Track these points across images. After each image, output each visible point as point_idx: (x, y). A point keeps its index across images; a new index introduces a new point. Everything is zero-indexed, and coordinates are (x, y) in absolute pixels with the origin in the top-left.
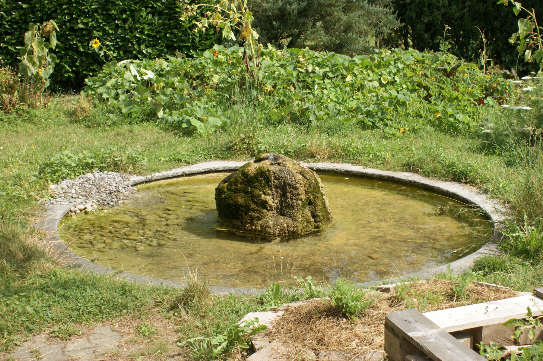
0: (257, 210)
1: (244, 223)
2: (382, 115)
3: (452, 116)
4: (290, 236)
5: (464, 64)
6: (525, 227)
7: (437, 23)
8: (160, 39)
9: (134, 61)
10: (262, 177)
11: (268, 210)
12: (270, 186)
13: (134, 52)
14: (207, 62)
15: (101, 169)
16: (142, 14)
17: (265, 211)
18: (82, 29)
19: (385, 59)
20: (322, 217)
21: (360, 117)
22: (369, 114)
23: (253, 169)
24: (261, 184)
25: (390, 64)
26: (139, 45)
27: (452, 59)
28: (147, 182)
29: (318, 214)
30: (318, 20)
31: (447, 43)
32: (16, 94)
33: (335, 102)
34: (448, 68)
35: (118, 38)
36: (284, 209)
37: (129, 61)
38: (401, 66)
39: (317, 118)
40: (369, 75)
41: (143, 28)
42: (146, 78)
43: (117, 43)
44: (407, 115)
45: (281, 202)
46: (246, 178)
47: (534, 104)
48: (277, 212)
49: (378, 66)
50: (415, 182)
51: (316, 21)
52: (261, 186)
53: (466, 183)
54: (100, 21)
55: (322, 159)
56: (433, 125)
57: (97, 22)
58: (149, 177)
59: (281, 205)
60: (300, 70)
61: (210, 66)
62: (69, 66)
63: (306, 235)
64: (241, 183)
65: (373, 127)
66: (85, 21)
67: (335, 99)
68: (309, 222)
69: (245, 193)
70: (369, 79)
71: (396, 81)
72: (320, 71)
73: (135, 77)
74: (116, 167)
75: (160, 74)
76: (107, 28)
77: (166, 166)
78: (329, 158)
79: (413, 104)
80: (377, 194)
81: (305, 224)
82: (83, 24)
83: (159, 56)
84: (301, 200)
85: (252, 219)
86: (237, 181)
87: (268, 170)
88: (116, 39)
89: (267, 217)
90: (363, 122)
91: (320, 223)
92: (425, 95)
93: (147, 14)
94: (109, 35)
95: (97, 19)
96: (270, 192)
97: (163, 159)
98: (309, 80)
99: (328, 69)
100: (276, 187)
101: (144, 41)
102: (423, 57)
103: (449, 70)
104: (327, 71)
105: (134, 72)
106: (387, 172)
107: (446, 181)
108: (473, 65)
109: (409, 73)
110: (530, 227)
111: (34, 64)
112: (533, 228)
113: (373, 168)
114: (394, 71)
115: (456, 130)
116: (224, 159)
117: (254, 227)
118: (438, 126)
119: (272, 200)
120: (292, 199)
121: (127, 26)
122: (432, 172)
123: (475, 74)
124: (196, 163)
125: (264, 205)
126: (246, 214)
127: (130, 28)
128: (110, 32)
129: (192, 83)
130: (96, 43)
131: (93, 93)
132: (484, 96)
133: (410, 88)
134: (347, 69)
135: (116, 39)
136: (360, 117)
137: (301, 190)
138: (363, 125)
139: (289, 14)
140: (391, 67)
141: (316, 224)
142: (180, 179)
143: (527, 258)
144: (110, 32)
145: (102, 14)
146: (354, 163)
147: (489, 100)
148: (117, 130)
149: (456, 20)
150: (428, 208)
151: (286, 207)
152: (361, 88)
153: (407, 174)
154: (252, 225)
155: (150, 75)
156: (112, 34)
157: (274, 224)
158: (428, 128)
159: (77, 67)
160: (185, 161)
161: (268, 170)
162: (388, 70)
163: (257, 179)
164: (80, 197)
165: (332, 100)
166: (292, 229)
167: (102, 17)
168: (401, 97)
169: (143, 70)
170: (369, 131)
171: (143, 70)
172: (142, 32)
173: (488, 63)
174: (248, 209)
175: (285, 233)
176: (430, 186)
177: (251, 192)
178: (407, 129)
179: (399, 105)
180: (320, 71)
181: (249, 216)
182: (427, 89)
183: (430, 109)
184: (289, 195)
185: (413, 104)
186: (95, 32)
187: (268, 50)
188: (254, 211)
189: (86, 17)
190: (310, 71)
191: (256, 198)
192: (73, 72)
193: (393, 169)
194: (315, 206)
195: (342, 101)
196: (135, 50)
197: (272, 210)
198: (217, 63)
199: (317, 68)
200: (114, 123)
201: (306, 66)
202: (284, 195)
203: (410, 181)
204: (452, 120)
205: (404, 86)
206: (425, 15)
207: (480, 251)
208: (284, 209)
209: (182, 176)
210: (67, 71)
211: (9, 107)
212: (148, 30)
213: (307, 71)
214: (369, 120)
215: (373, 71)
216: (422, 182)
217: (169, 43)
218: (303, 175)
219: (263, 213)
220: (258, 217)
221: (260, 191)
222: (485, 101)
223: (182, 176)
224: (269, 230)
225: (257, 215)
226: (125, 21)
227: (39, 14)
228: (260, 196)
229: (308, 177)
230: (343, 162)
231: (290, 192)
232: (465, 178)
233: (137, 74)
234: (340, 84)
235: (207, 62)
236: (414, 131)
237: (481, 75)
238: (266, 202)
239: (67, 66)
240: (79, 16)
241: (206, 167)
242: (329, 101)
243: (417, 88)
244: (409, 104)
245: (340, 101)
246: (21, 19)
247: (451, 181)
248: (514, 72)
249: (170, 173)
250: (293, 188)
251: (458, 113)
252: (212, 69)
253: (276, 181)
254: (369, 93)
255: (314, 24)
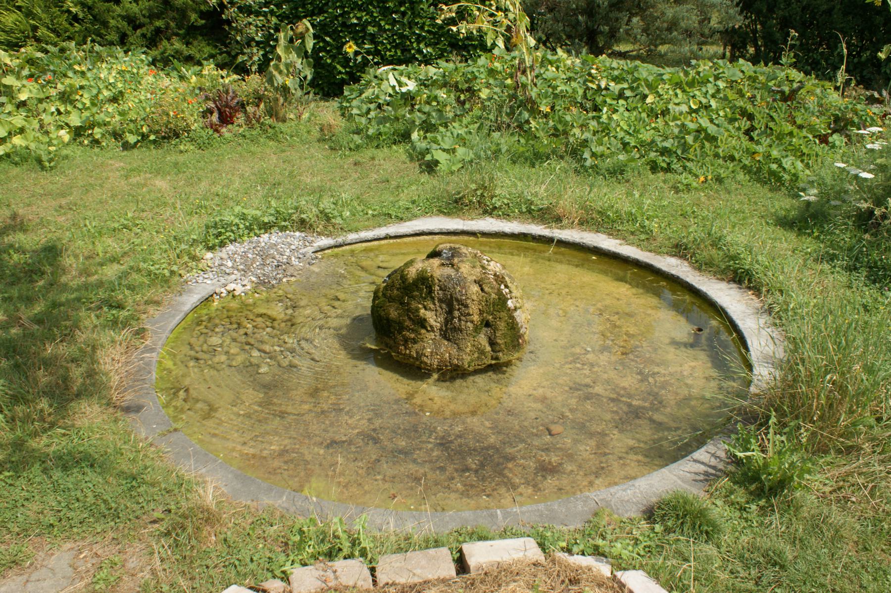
0: (413, 330)
1: (397, 345)
2: (682, 153)
3: (778, 161)
4: (453, 373)
5: (812, 82)
6: (770, 436)
7: (795, 19)
8: (442, 36)
9: (397, 67)
10: (423, 284)
11: (428, 331)
12: (433, 298)
13: (413, 52)
14: (479, 71)
15: (283, 229)
16: (422, 6)
17: (423, 331)
18: (356, 25)
19: (701, 75)
20: (503, 346)
21: (653, 155)
22: (664, 152)
23: (414, 270)
24: (421, 294)
25: (708, 81)
26: (419, 43)
27: (796, 75)
28: (336, 247)
29: (498, 341)
30: (636, 14)
31: (792, 55)
32: (262, 106)
33: (626, 131)
34: (786, 89)
35: (396, 34)
36: (449, 332)
37: (391, 67)
38: (721, 84)
39: (594, 155)
40: (676, 95)
41: (424, 24)
42: (404, 90)
43: (394, 40)
44: (716, 155)
45: (447, 321)
46: (403, 282)
47: (882, 168)
48: (441, 334)
49: (691, 84)
50: (678, 277)
51: (632, 15)
52: (421, 297)
53: (749, 288)
54: (375, 15)
55: (571, 226)
56: (749, 172)
57: (372, 16)
58: (340, 240)
59: (446, 326)
60: (590, 85)
61: (482, 76)
62: (342, 66)
63: (476, 372)
64: (398, 289)
65: (668, 169)
66: (359, 15)
67: (625, 127)
68: (482, 352)
69: (401, 304)
70: (677, 101)
71: (711, 106)
72: (615, 87)
73: (393, 87)
74: (303, 225)
75: (423, 84)
76: (383, 23)
77: (371, 223)
78: (581, 223)
79: (726, 139)
80: (621, 293)
81: (476, 355)
82: (358, 18)
83: (441, 57)
84: (472, 322)
85: (406, 340)
86: (393, 286)
87: (432, 276)
88: (393, 35)
89: (425, 340)
90: (654, 162)
91: (501, 354)
92: (746, 128)
93: (429, 7)
94: (385, 31)
95: (372, 12)
96: (432, 306)
97: (370, 212)
98: (599, 99)
99: (625, 85)
100: (440, 301)
101: (424, 38)
102: (755, 72)
103: (787, 92)
104: (624, 89)
105: (393, 82)
106: (648, 254)
107: (723, 280)
108: (827, 84)
109: (731, 95)
110: (778, 436)
111: (280, 72)
112: (784, 438)
113: (632, 244)
114: (711, 92)
115: (779, 179)
116: (448, 214)
117: (408, 352)
118: (755, 174)
119: (433, 317)
120: (460, 320)
121: (405, 21)
122: (706, 264)
123: (827, 96)
124: (410, 220)
125: (422, 323)
126: (400, 333)
127: (409, 23)
128: (387, 27)
129: (459, 97)
130: (350, 47)
131: (348, 105)
132: (830, 131)
133: (729, 116)
134: (650, 86)
135: (393, 35)
136: (653, 155)
137: (474, 309)
138: (654, 167)
139: (599, 6)
140: (709, 85)
141: (495, 355)
142: (383, 242)
143: (759, 494)
144: (387, 27)
145: (379, 7)
146: (611, 235)
147: (836, 138)
148: (357, 157)
149: (821, 15)
150: (682, 329)
151: (451, 329)
152: (665, 112)
153: (673, 261)
154: (406, 348)
155: (411, 86)
156: (389, 30)
157: (432, 353)
158: (741, 176)
159: (351, 67)
160: (396, 217)
161: (432, 276)
162: (704, 90)
163: (417, 286)
164: (236, 272)
165: (622, 129)
166: (455, 361)
167: (378, 10)
168: (712, 129)
169: (404, 79)
170: (661, 175)
171: (404, 79)
172: (422, 28)
173: (847, 83)
174: (402, 328)
175: (446, 366)
176: (696, 288)
177: (408, 304)
178: (710, 177)
179: (708, 140)
180: (615, 87)
181: (404, 336)
182: (751, 117)
183: (747, 149)
184: (456, 313)
185: (726, 139)
186: (369, 28)
187: (555, 57)
188: (409, 330)
189: (360, 10)
190: (603, 86)
191: (413, 313)
192: (347, 73)
193: (657, 251)
194: (495, 330)
195: (634, 131)
196: (413, 49)
197: (433, 331)
198: (492, 72)
199: (612, 84)
200: (358, 147)
201: (599, 81)
202: (450, 312)
203: (672, 275)
204: (774, 167)
205: (721, 113)
206: (780, 9)
207: (697, 455)
208: (449, 332)
209: (385, 238)
210: (340, 73)
211: (254, 122)
212: (429, 26)
213: (599, 86)
214: (664, 160)
215: (684, 91)
216: (688, 280)
217: (453, 40)
218: (480, 286)
219: (420, 334)
220: (414, 339)
221: (419, 303)
222: (830, 139)
223: (385, 238)
224: (425, 359)
225: (413, 336)
226: (404, 14)
227: (309, 7)
228: (418, 310)
229: (486, 289)
230: (597, 231)
231: (459, 310)
232: (750, 281)
233: (396, 84)
234: (639, 106)
235: (479, 71)
236: (719, 180)
237: (834, 97)
238: (425, 320)
239: (338, 67)
240: (352, 9)
241: (417, 228)
242: (618, 129)
243: (738, 117)
244: (721, 140)
245: (631, 131)
246: (292, 14)
247: (729, 282)
248: (884, 93)
249: (369, 234)
250: (462, 304)
251: (787, 156)
252: (484, 81)
253: (440, 292)
254: (672, 121)
255: (629, 20)
